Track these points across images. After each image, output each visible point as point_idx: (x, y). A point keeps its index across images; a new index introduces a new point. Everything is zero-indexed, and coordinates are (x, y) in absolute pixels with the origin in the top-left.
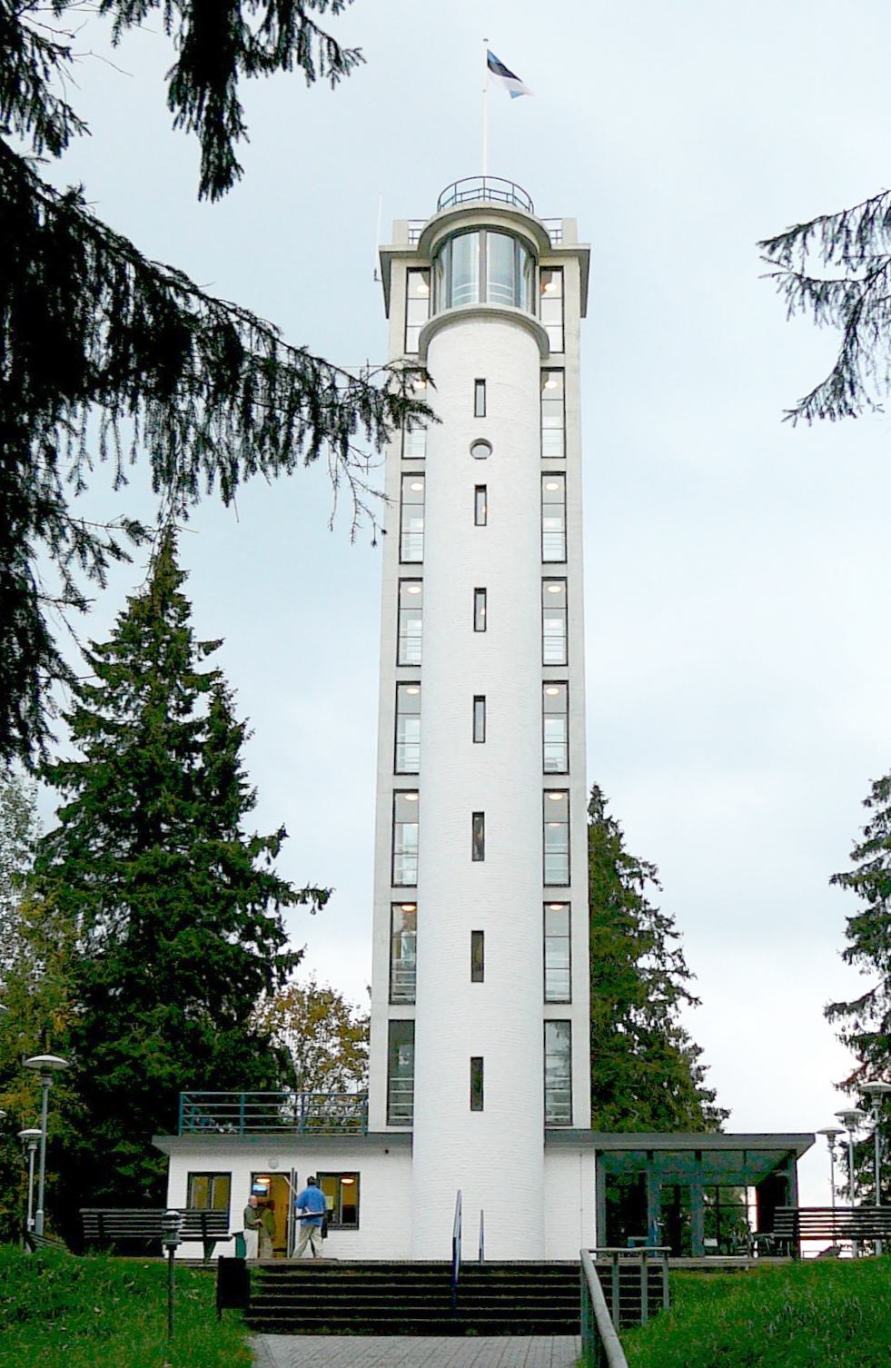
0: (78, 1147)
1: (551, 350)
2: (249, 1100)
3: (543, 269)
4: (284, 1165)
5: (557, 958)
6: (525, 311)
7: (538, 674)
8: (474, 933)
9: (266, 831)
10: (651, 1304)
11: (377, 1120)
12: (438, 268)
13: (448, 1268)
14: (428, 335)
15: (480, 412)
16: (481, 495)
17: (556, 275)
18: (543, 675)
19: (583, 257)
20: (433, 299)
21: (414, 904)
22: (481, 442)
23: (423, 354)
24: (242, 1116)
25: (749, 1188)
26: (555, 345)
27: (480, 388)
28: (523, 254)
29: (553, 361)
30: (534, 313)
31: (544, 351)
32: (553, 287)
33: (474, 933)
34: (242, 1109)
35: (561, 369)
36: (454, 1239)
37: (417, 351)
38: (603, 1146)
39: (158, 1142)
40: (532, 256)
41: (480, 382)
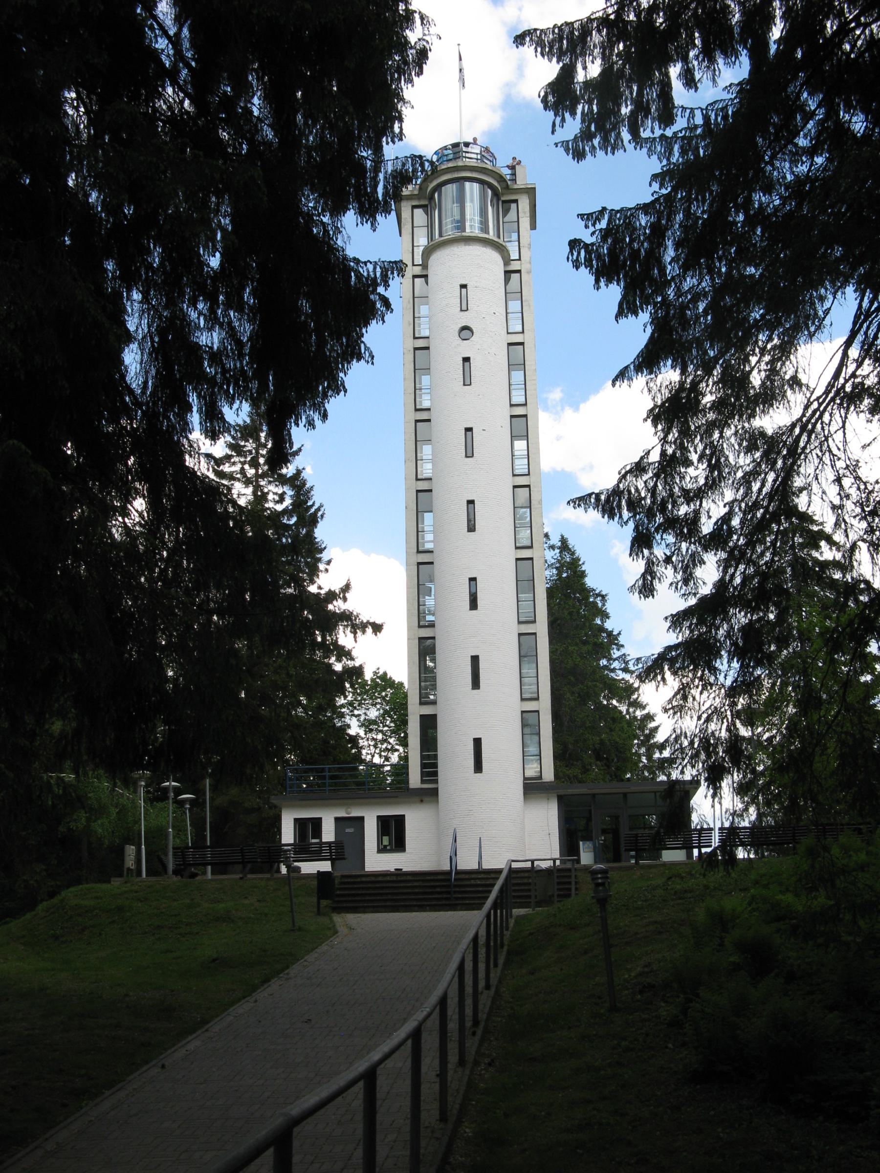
0: (28, 729)
1: (512, 258)
2: (330, 770)
3: (504, 202)
4: (355, 813)
5: (529, 670)
6: (492, 235)
7: (510, 482)
8: (472, 657)
9: (336, 587)
10: (576, 889)
11: (415, 779)
12: (433, 204)
13: (449, 873)
14: (428, 252)
15: (464, 308)
16: (467, 364)
17: (513, 206)
18: (513, 482)
19: (531, 192)
20: (430, 226)
21: (433, 638)
22: (465, 328)
23: (425, 266)
24: (327, 774)
25: (329, 863)
26: (514, 255)
27: (464, 290)
28: (490, 192)
29: (514, 266)
30: (499, 237)
31: (507, 261)
32: (512, 216)
33: (472, 657)
34: (327, 777)
35: (519, 271)
36: (451, 858)
37: (421, 263)
38: (562, 792)
39: (274, 800)
40: (496, 194)
41: (463, 286)
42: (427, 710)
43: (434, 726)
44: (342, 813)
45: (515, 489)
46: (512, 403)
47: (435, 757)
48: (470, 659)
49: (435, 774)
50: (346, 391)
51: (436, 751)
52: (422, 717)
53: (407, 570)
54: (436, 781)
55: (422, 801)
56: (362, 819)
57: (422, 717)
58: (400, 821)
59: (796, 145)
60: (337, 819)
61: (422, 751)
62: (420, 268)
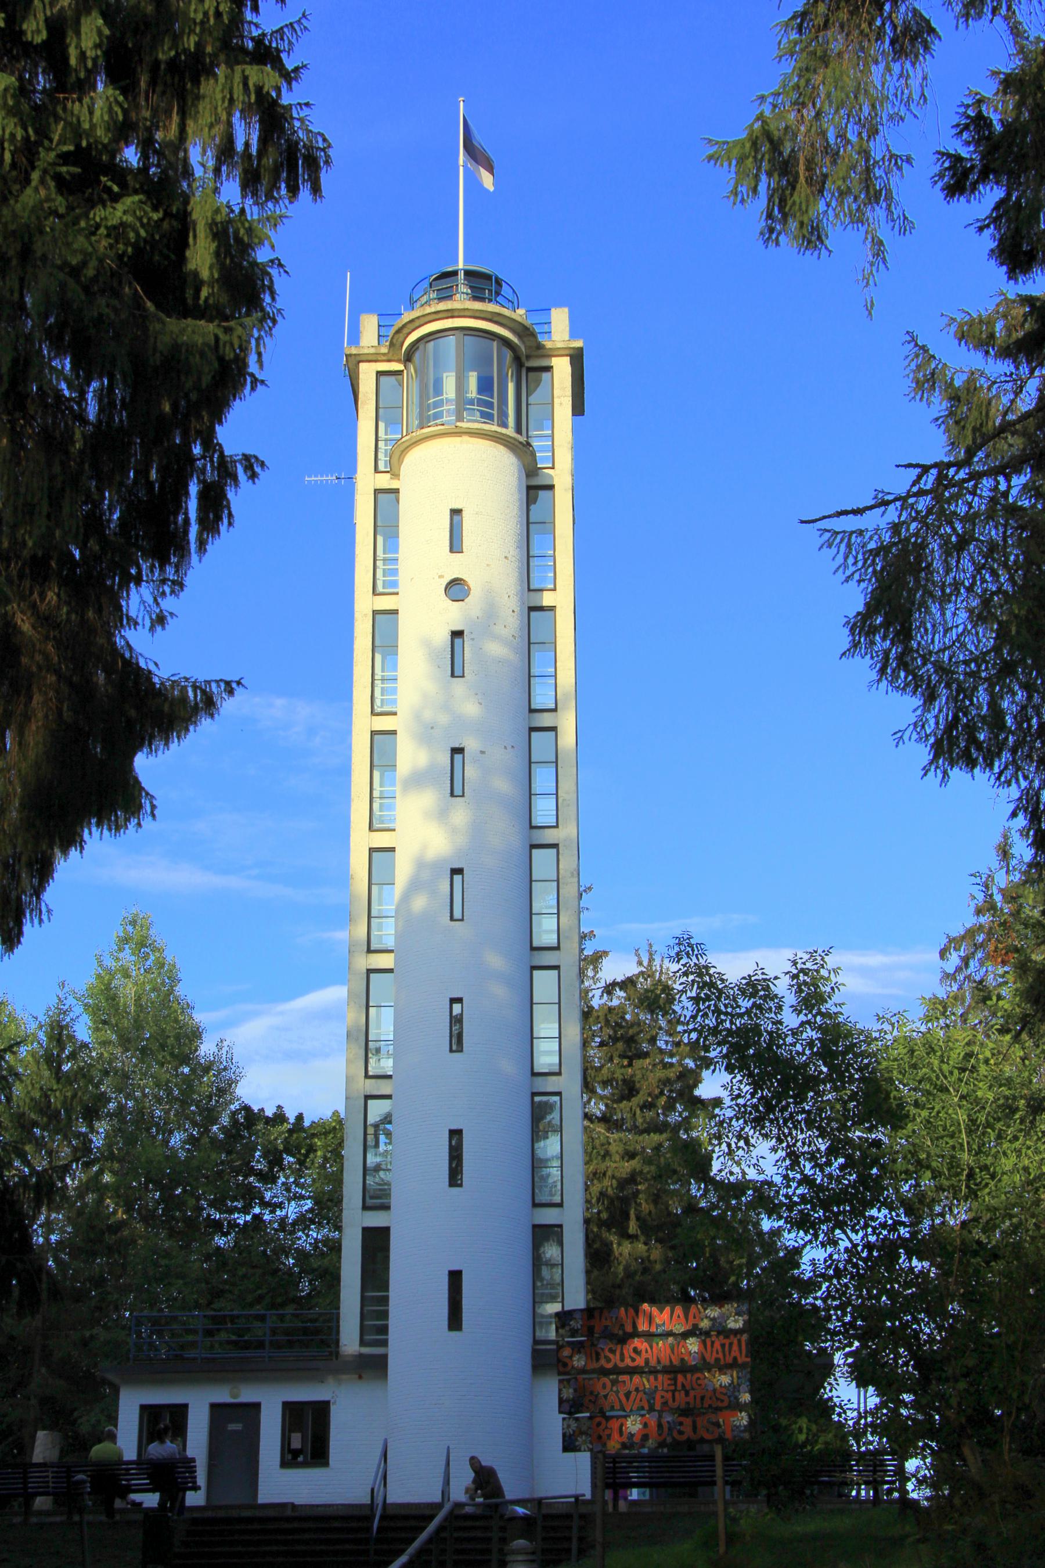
3: (530, 369)
4: (247, 1394)
15: (457, 914)
40: (518, 361)
42: (376, 1220)
43: (385, 1248)
44: (222, 1395)
45: (532, 614)
46: (533, 707)
47: (385, 1300)
48: (446, 1278)
49: (384, 1330)
50: (262, 464)
51: (387, 1289)
52: (366, 1231)
53: (349, 863)
54: (385, 1343)
55: (360, 1377)
56: (257, 1406)
57: (366, 1231)
58: (321, 1411)
59: (984, 741)
60: (214, 1407)
61: (364, 1288)
62: (388, 475)
